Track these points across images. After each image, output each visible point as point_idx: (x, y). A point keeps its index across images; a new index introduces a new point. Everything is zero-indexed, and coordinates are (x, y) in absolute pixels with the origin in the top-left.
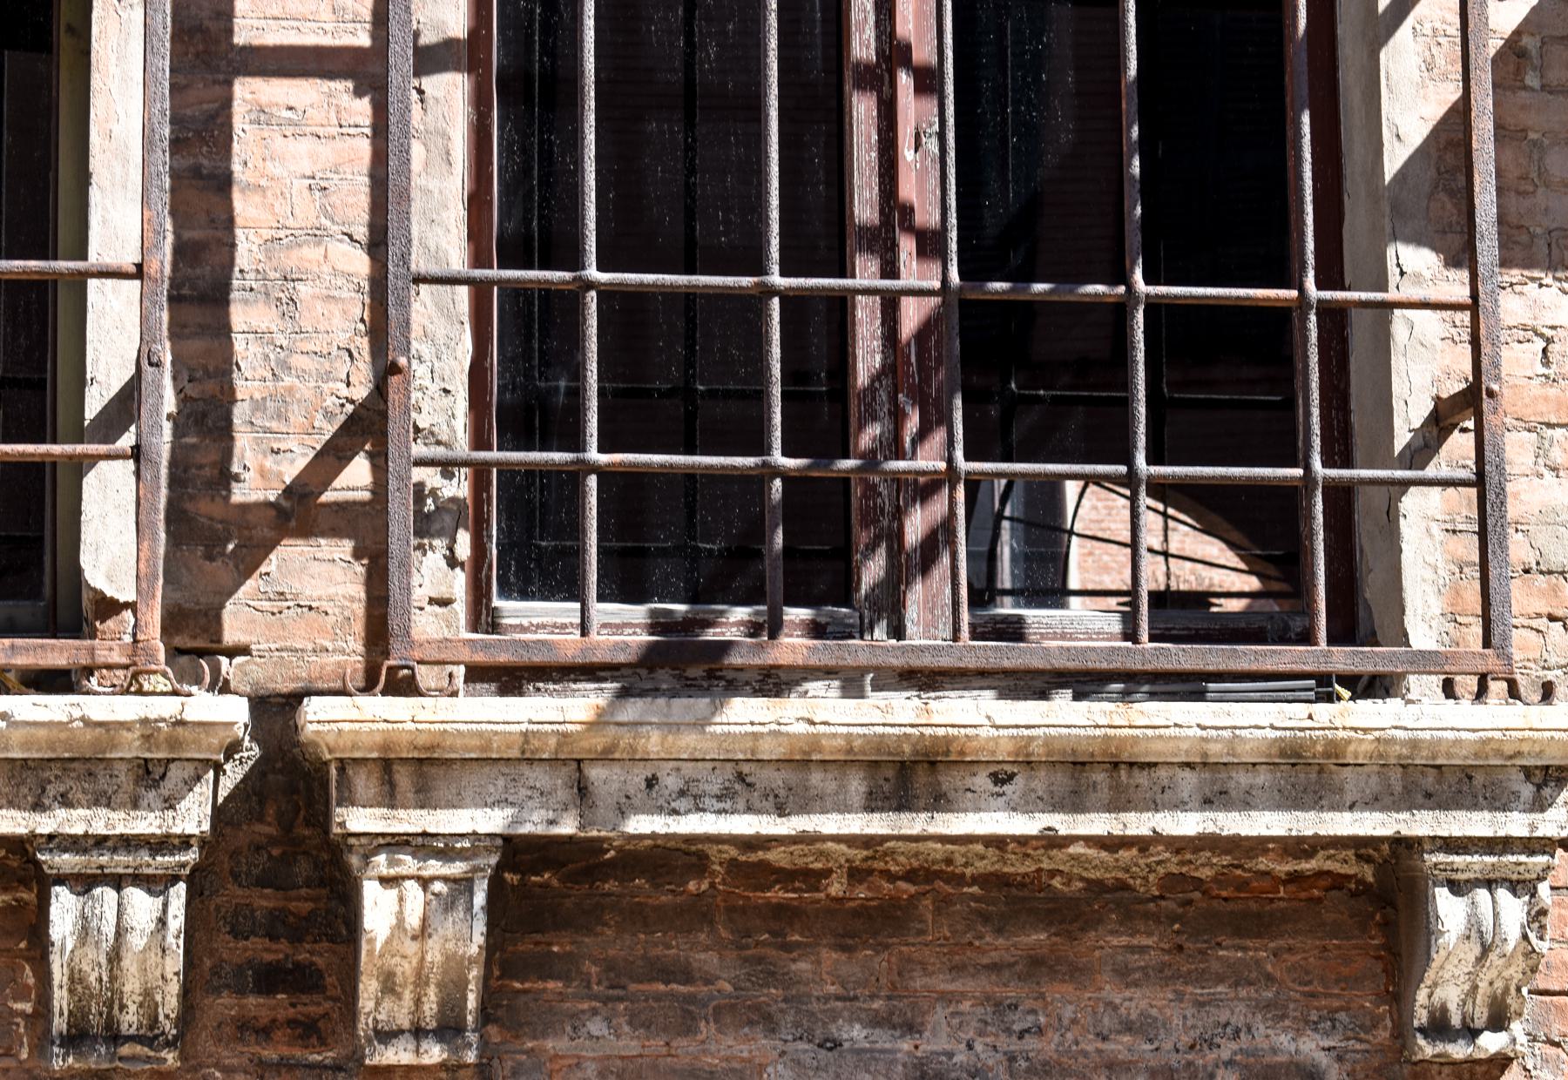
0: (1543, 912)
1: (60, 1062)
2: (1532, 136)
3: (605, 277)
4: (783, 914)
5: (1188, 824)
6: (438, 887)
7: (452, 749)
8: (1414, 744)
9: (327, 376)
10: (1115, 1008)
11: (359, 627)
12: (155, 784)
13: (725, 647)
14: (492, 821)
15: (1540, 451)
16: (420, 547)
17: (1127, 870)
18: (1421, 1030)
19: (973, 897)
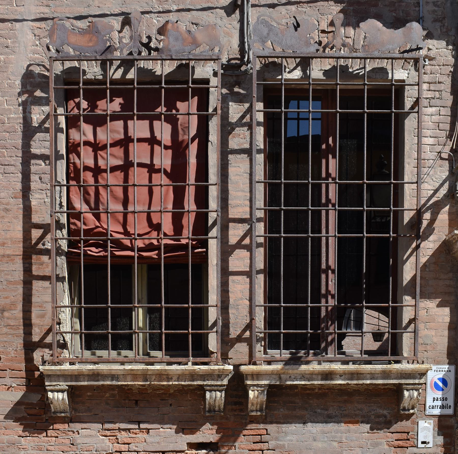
0: (420, 393)
1: (207, 414)
2: (427, 278)
3: (284, 305)
4: (308, 394)
5: (368, 382)
6: (260, 391)
7: (262, 373)
8: (402, 370)
9: (243, 319)
10: (357, 407)
11: (248, 355)
12: (220, 378)
13: (301, 357)
14: (266, 382)
15: (425, 326)
16: (257, 344)
17: (359, 388)
18: (401, 410)
19: (336, 392)
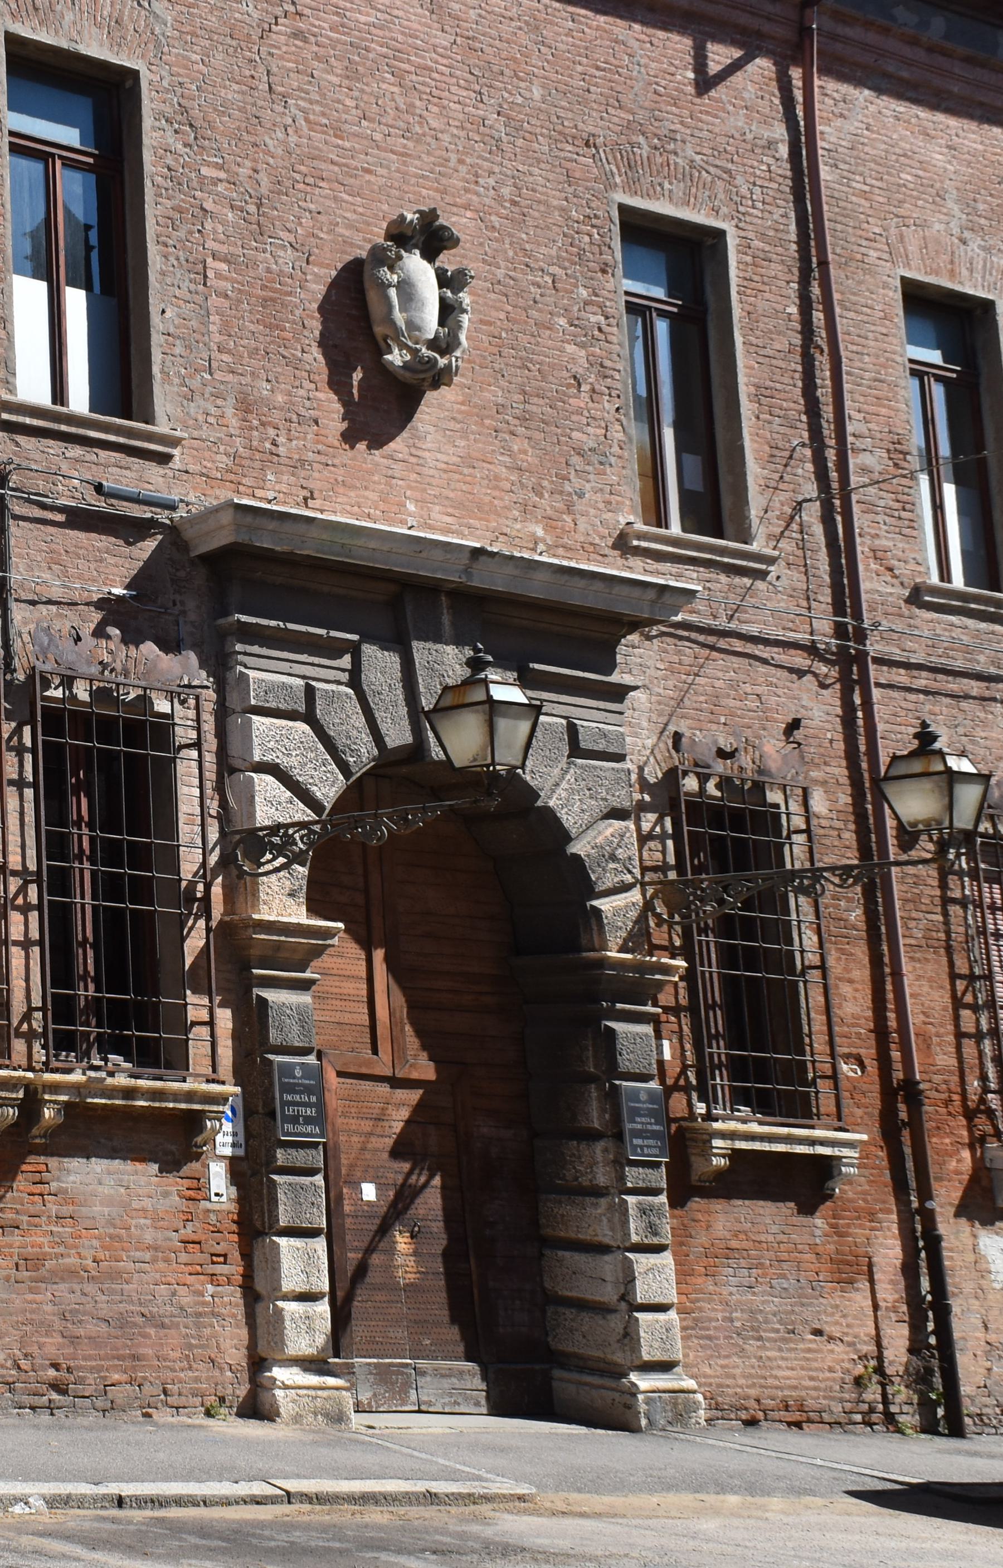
5: (171, 1105)
